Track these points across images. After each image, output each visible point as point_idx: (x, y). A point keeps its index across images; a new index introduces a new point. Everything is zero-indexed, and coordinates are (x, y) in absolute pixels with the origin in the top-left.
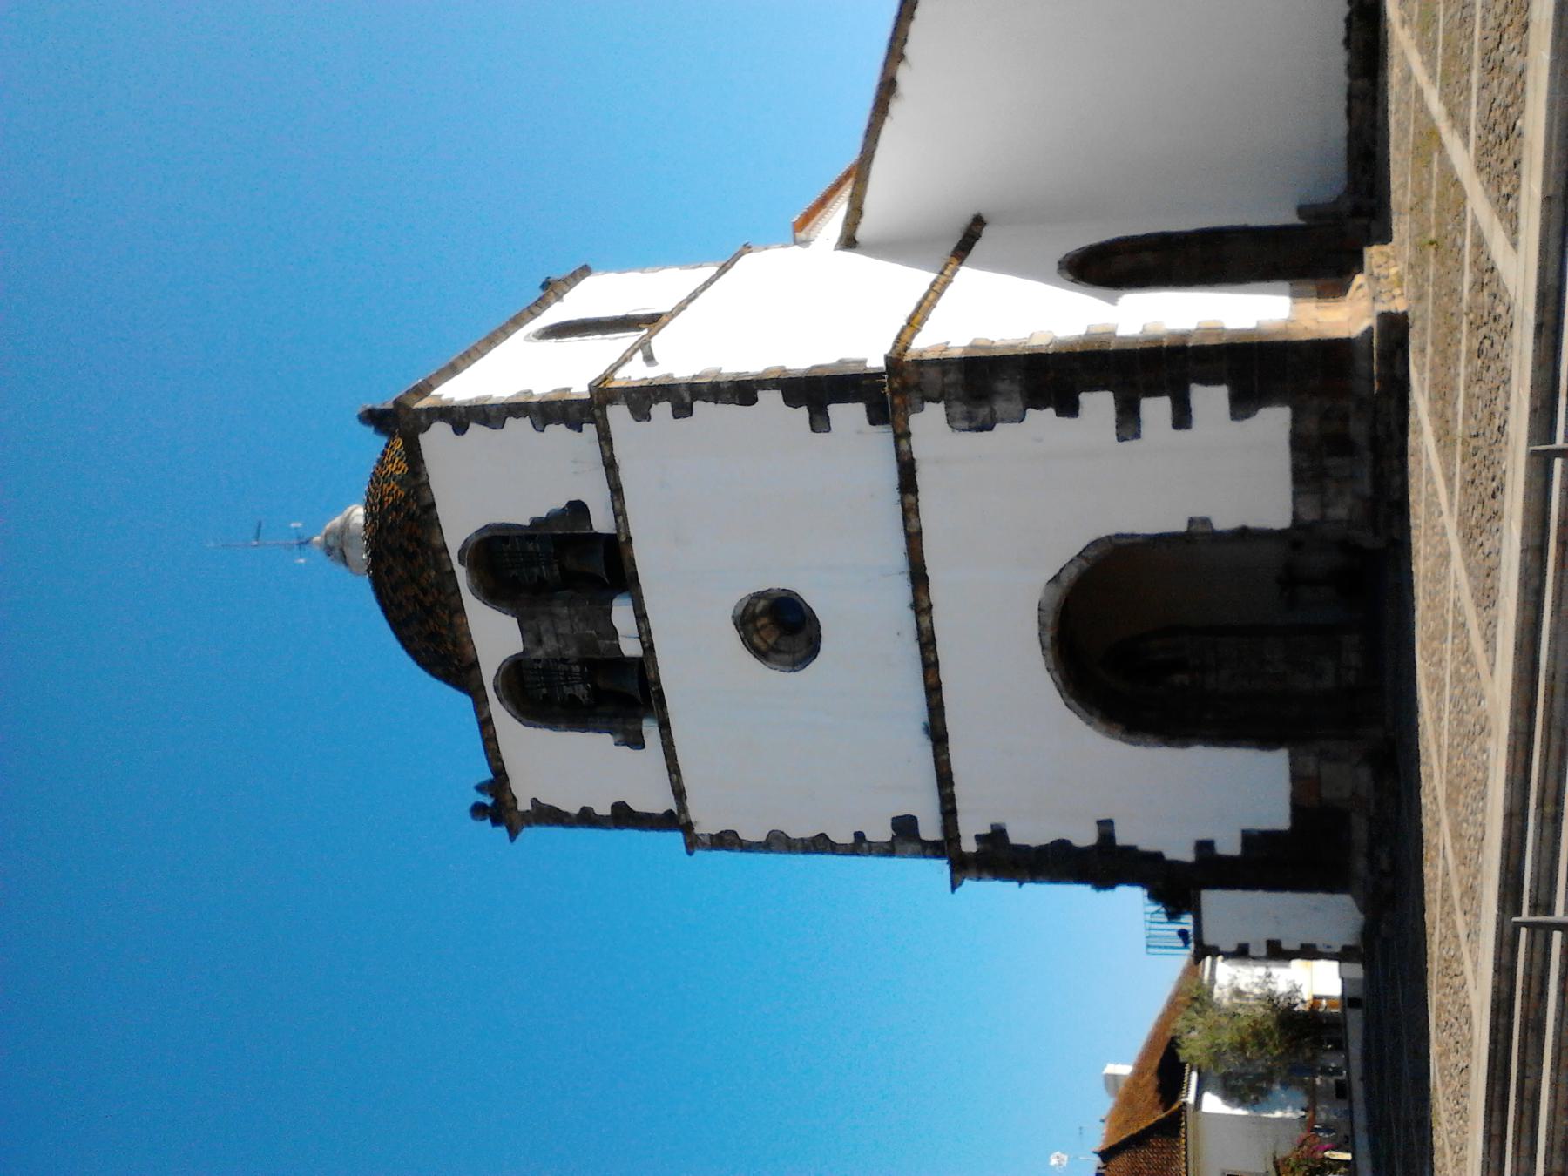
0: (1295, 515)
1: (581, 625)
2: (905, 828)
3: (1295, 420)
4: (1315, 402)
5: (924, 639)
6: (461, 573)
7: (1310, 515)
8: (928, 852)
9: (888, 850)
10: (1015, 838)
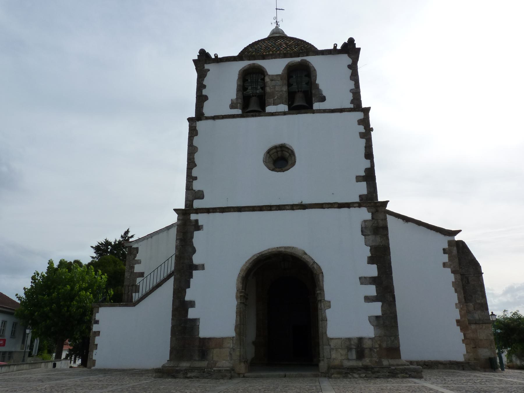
0: (332, 339)
1: (279, 95)
2: (200, 195)
4: (377, 346)
5: (188, 202)
6: (298, 59)
7: (332, 344)
8: (188, 202)
9: (189, 188)
10: (197, 234)
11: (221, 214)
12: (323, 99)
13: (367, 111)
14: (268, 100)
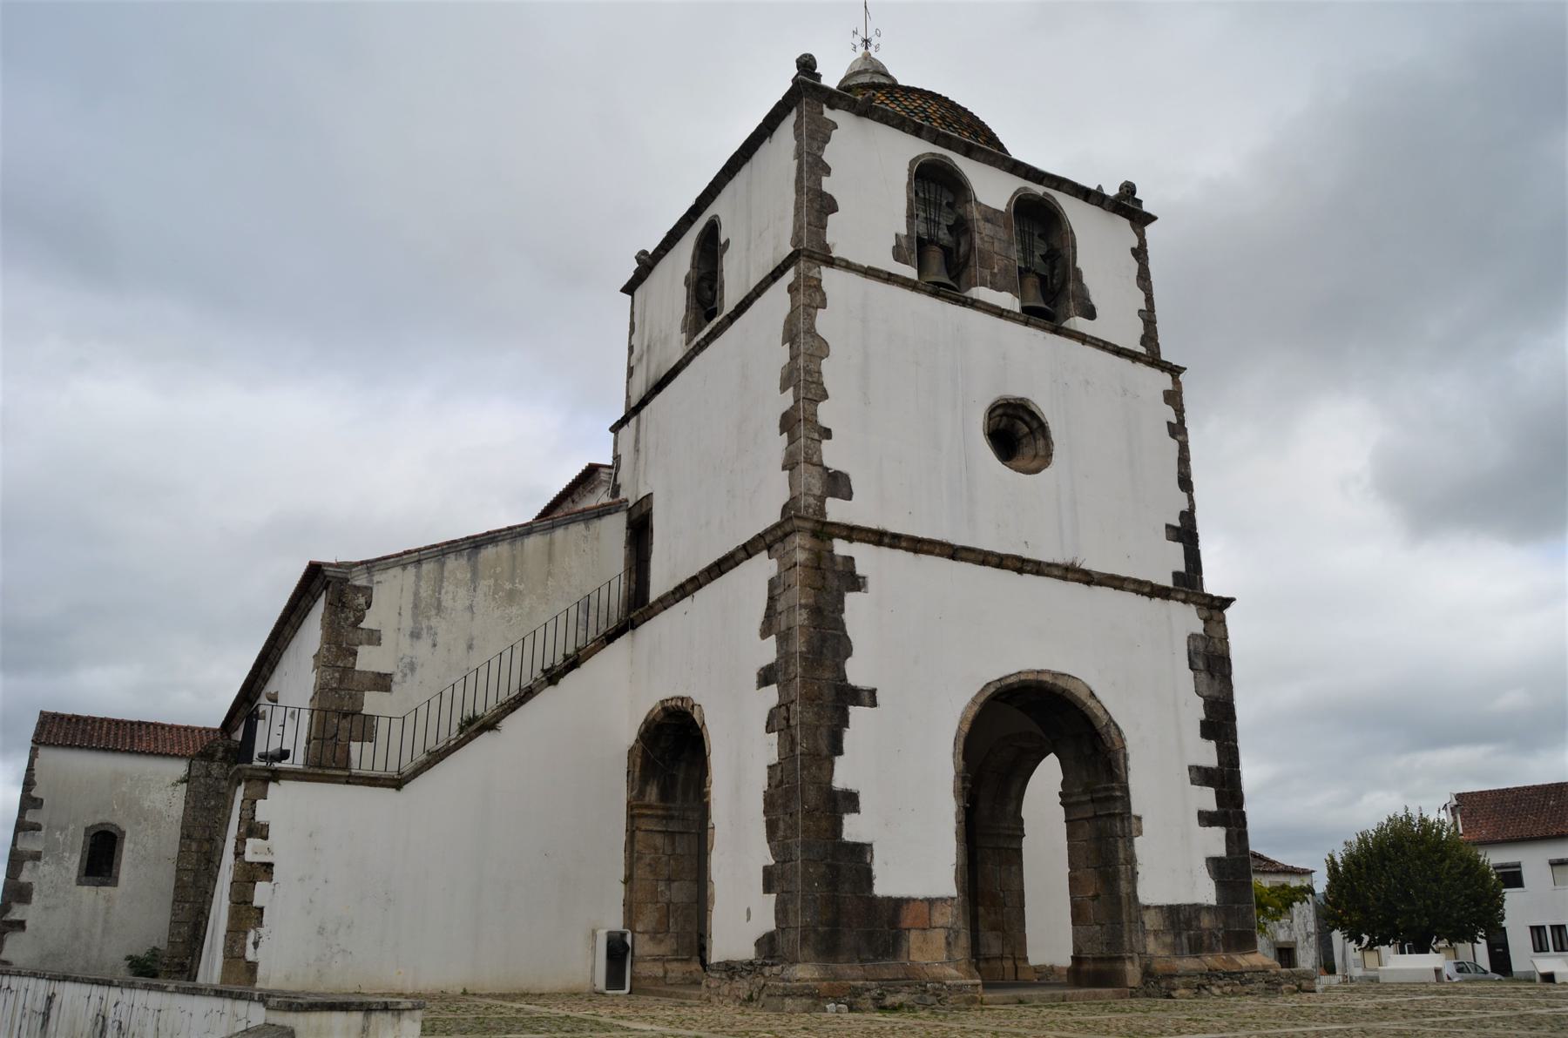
0: (1148, 907)
3: (1209, 908)
7: (1151, 921)
11: (911, 554)
12: (1090, 313)
13: (1175, 371)
14: (977, 270)
